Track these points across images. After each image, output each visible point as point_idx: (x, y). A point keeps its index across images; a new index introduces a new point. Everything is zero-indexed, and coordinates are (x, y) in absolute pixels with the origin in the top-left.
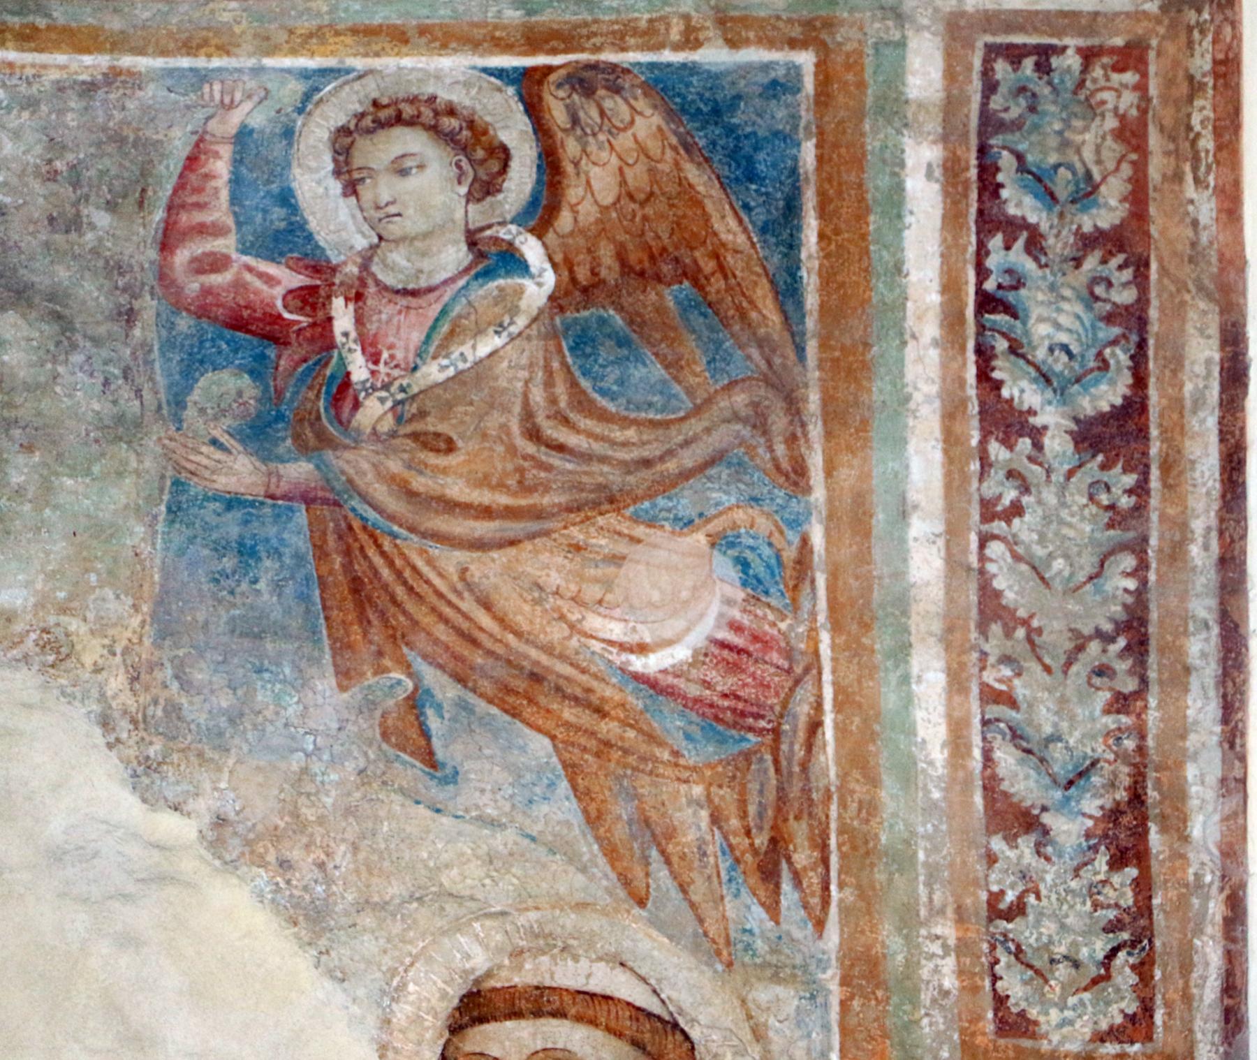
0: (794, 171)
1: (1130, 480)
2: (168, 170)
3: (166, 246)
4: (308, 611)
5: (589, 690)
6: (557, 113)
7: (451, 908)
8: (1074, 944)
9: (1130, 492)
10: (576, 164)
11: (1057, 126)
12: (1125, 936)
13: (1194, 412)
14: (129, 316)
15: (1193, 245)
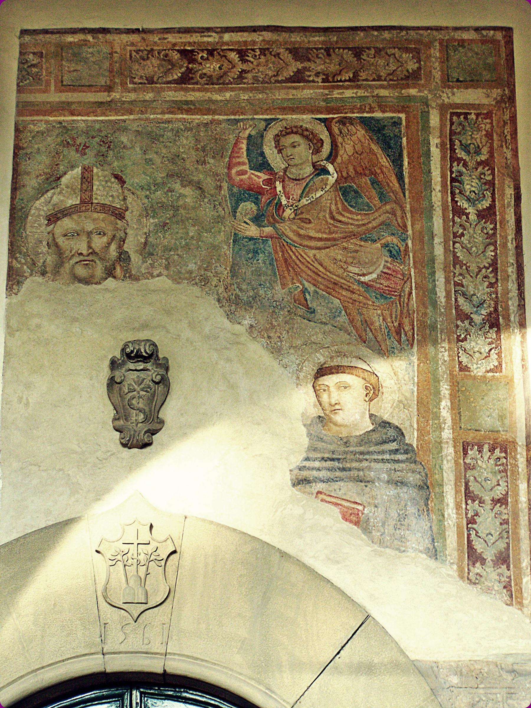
0: (401, 146)
1: (492, 226)
3: (229, 168)
4: (273, 268)
5: (349, 287)
6: (336, 130)
7: (314, 346)
8: (480, 348)
9: (492, 229)
10: (342, 144)
11: (470, 134)
12: (494, 346)
13: (508, 207)
15: (506, 164)
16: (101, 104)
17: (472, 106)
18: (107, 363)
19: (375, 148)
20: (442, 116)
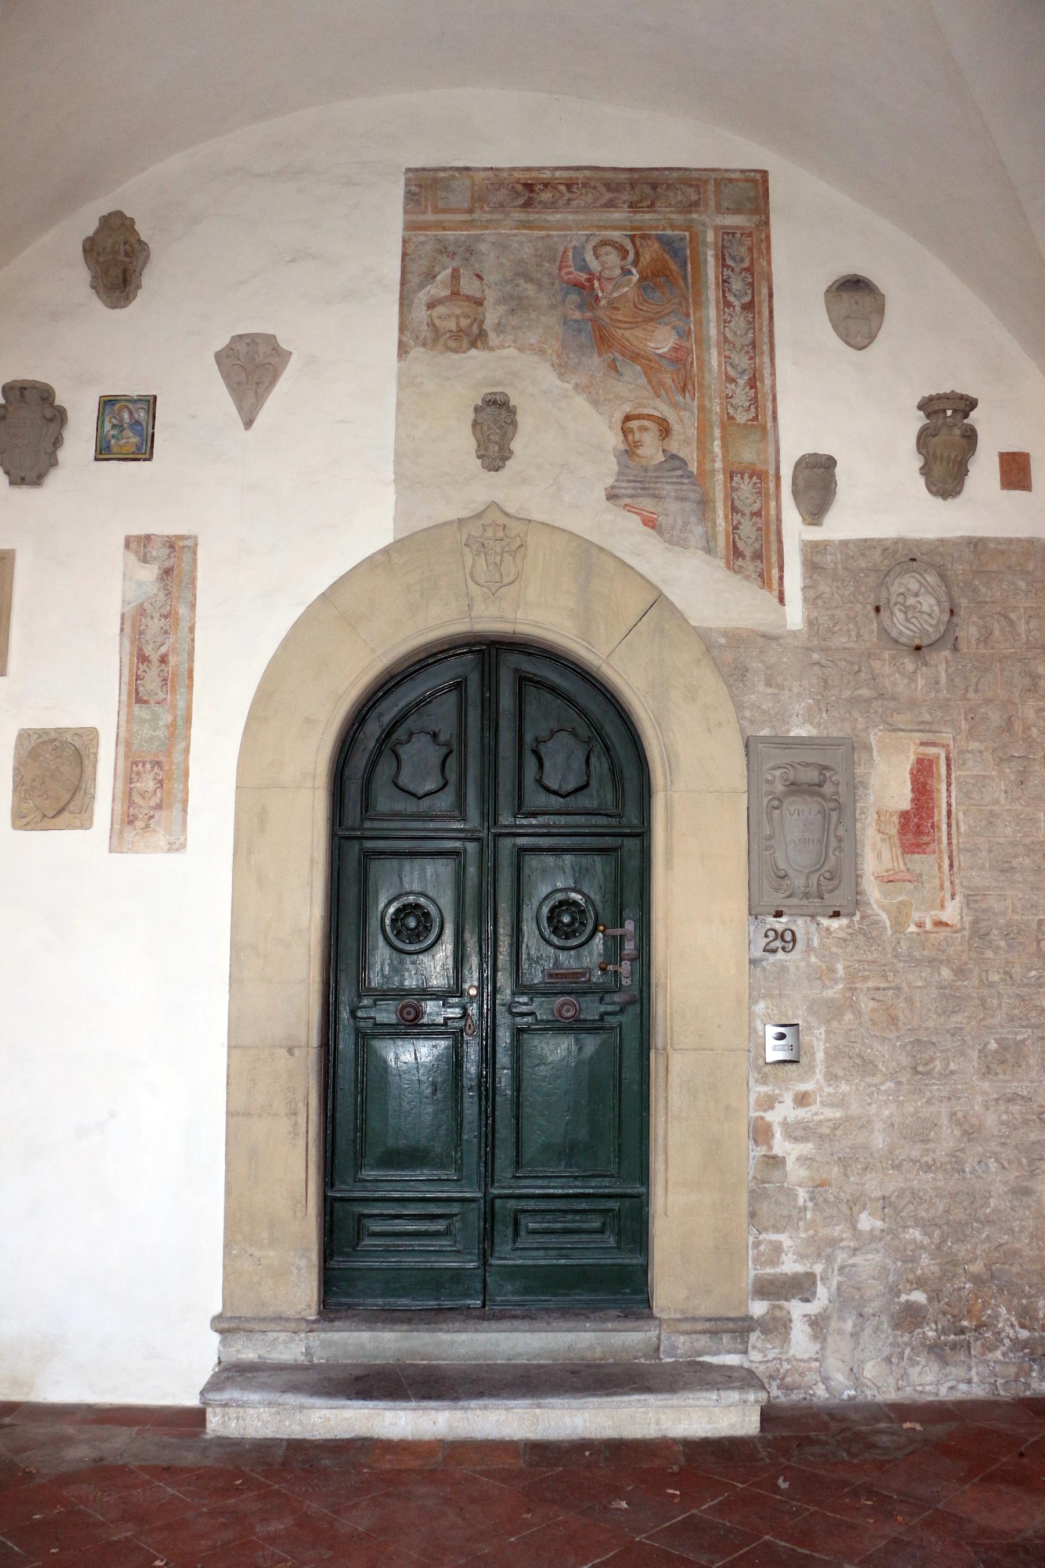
2: (560, 254)
3: (560, 270)
6: (638, 244)
14: (553, 284)
16: (465, 222)
17: (737, 227)
18: (472, 409)
19: (667, 257)
20: (716, 234)
